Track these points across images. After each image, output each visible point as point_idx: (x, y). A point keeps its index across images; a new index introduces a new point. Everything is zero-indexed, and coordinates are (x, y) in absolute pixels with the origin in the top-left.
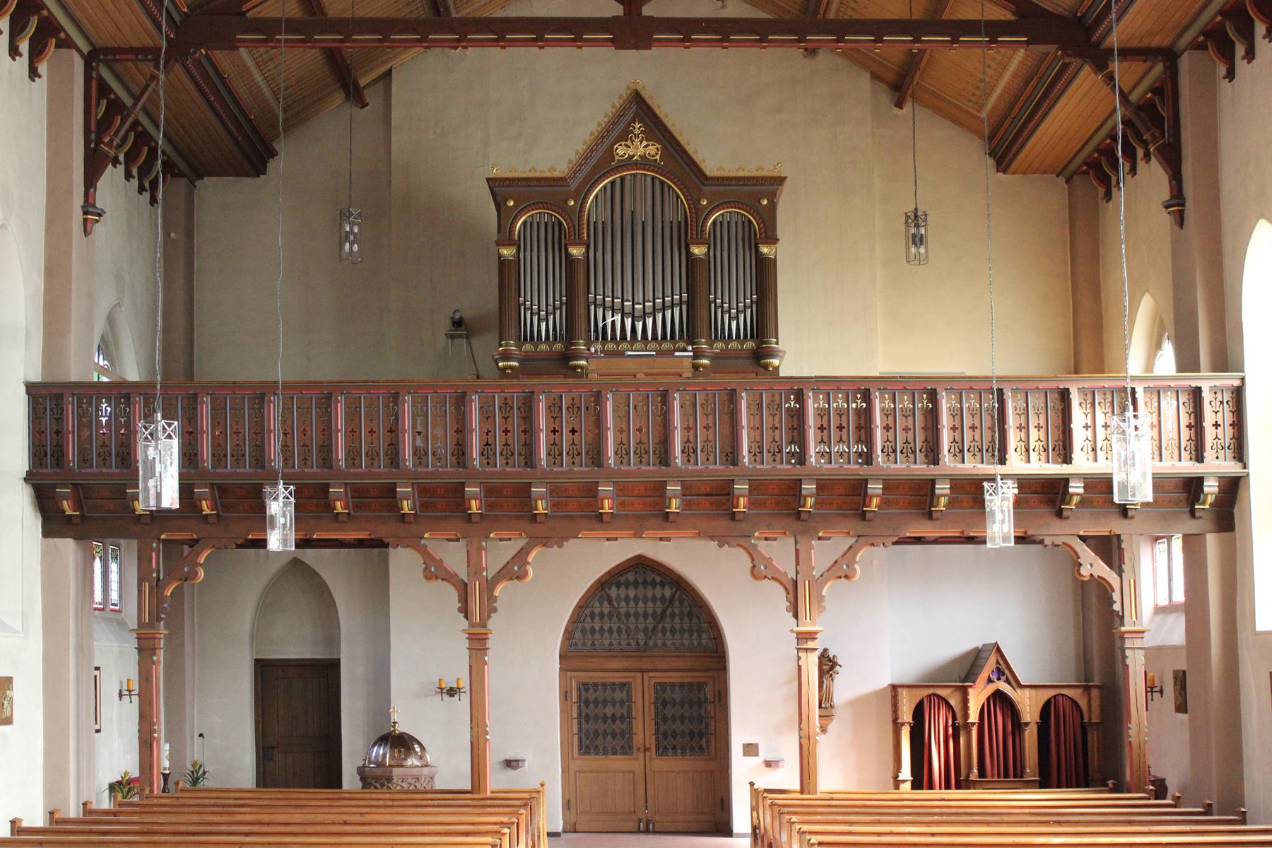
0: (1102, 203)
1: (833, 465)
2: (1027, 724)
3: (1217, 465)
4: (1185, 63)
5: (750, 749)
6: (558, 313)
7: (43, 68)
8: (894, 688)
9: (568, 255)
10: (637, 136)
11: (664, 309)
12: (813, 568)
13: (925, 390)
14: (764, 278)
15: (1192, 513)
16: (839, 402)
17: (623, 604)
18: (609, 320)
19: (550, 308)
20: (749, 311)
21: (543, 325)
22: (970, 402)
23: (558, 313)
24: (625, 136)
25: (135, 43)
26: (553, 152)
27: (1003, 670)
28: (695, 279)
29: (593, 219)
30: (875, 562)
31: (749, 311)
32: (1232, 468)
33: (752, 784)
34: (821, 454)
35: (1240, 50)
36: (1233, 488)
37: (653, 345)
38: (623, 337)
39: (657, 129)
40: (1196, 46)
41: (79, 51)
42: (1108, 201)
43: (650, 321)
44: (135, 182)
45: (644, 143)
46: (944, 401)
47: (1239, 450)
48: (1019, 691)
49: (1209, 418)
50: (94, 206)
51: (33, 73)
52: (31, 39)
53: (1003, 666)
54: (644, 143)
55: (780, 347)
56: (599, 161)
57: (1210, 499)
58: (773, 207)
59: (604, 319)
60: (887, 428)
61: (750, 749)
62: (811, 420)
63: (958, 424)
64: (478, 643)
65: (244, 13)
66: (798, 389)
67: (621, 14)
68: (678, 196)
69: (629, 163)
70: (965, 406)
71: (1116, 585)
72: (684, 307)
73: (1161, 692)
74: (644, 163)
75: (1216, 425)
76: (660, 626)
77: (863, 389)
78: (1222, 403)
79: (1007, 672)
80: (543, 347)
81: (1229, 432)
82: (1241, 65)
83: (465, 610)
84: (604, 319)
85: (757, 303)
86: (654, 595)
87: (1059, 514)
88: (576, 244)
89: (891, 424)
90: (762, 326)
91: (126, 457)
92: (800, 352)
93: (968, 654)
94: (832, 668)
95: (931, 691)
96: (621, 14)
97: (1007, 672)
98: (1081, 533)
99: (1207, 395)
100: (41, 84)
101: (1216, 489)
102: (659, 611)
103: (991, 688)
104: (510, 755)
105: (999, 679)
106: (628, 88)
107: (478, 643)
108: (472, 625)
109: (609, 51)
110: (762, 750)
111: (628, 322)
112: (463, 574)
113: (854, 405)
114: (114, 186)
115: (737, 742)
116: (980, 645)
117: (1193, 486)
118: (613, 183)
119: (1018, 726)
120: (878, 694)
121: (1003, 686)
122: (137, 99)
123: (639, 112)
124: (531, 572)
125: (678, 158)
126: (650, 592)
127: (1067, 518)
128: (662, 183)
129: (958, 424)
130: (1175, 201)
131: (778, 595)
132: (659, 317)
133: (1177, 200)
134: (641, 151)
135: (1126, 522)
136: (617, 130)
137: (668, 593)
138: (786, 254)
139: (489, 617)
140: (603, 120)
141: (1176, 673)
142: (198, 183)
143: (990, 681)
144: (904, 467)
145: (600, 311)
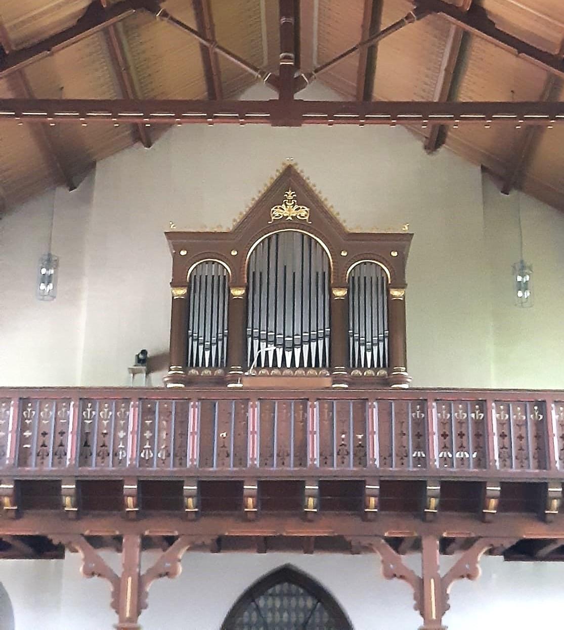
6: (220, 343)
10: (290, 201)
14: (395, 315)
16: (459, 413)
22: (517, 413)
23: (220, 343)
26: (222, 213)
28: (340, 318)
30: (494, 576)
34: (444, 460)
38: (275, 365)
39: (306, 196)
43: (297, 352)
46: (553, 412)
55: (281, 165)
56: (257, 218)
59: (259, 349)
60: (502, 436)
62: (435, 427)
67: (278, 99)
68: (323, 249)
69: (283, 222)
70: (513, 417)
72: (327, 340)
74: (296, 222)
77: (479, 400)
80: (207, 372)
83: (117, 605)
84: (259, 349)
85: (388, 337)
89: (507, 433)
90: (394, 357)
91: (5, 461)
92: (422, 371)
96: (278, 99)
106: (284, 164)
108: (122, 620)
109: (267, 127)
112: (119, 571)
113: (473, 415)
118: (269, 238)
123: (289, 181)
124: (180, 569)
128: (310, 238)
134: (294, 213)
138: (413, 296)
140: (263, 190)
144: (515, 471)
145: (256, 342)
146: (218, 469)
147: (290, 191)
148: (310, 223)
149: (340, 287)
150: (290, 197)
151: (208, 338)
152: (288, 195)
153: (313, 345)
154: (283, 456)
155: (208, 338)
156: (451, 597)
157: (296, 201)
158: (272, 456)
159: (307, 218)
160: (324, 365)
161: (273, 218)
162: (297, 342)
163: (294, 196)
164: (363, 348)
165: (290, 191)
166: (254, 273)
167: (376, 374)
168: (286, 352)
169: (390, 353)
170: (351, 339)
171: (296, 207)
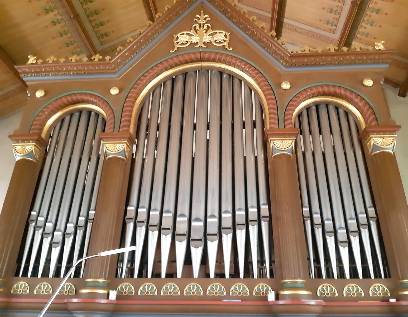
38: (171, 275)
147: (202, 15)
148: (231, 49)
149: (282, 135)
150: (202, 22)
151: (340, 222)
152: (199, 19)
153: (241, 235)
155: (340, 222)
156: (73, 227)
157: (209, 25)
159: (226, 44)
160: (261, 274)
161: (177, 46)
162: (197, 234)
163: (208, 19)
164: (331, 241)
165: (202, 15)
166: (149, 121)
167: (341, 292)
168: (193, 249)
169: (276, 242)
170: (308, 223)
171: (211, 32)
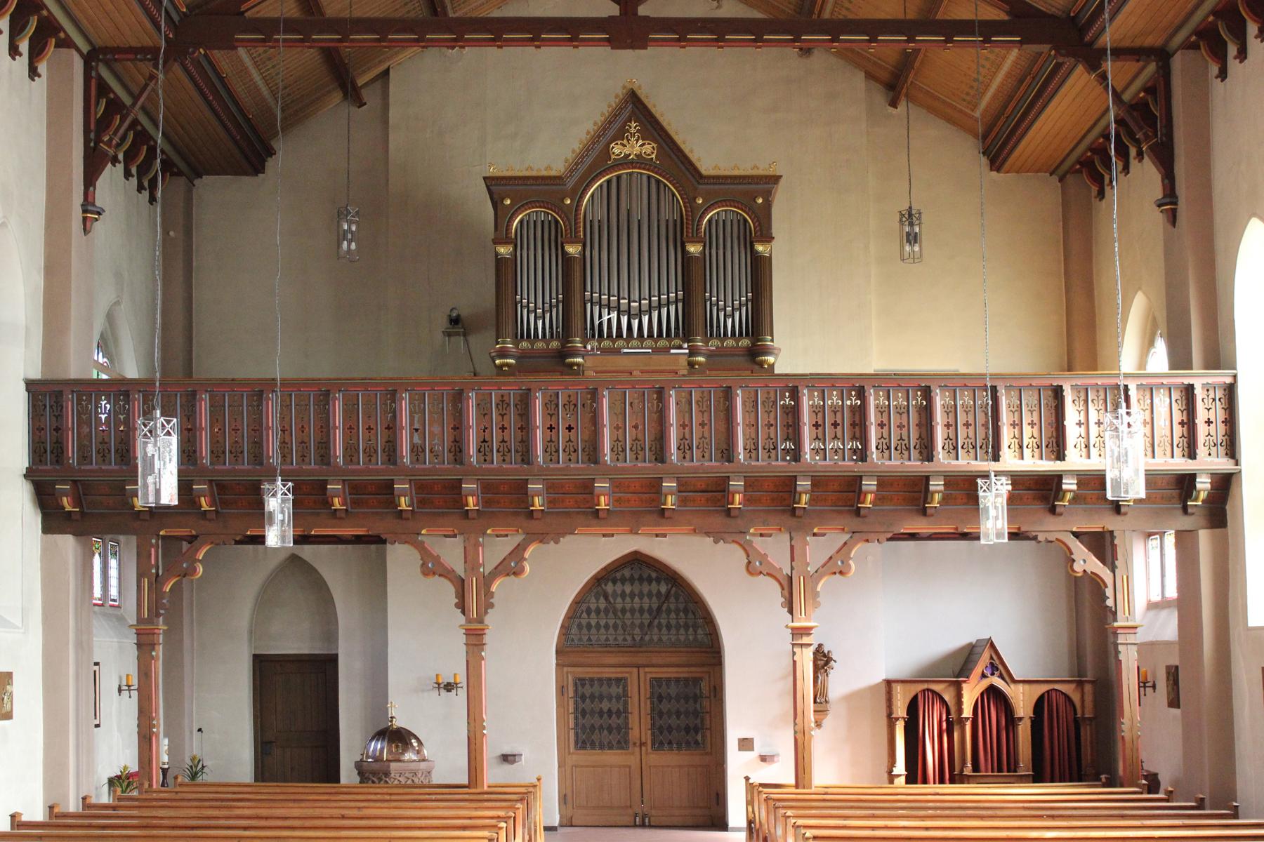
0: (1095, 202)
1: (828, 462)
2: (1020, 719)
3: (1209, 462)
4: (1177, 62)
5: (746, 744)
6: (554, 310)
7: (42, 68)
8: (889, 683)
9: (564, 253)
10: (633, 135)
11: (659, 307)
12: (808, 564)
13: (919, 388)
14: (759, 276)
15: (1185, 510)
16: (834, 399)
17: (619, 600)
18: (605, 318)
19: (547, 306)
20: (744, 309)
21: (540, 323)
22: (964, 399)
23: (554, 310)
24: (621, 135)
25: (134, 43)
26: (549, 151)
27: (997, 666)
28: (691, 277)
29: (589, 217)
30: (870, 558)
31: (744, 309)
32: (1224, 465)
33: (747, 779)
34: (816, 451)
35: (1232, 50)
36: (1225, 484)
37: (649, 343)
38: (619, 335)
39: (653, 128)
40: (1189, 46)
41: (78, 50)
42: (1101, 200)
43: (645, 319)
44: (134, 181)
45: (640, 142)
46: (938, 398)
47: (1231, 447)
48: (1012, 686)
49: (1201, 415)
50: (94, 205)
51: (33, 73)
52: (31, 39)
53: (997, 662)
54: (640, 142)
55: (776, 344)
56: (595, 160)
57: (1203, 496)
58: (768, 205)
59: (600, 317)
60: (881, 425)
61: (746, 744)
63: (952, 421)
64: (475, 638)
65: (243, 13)
66: (793, 386)
67: (617, 13)
68: (674, 195)
69: (625, 162)
71: (1109, 581)
72: (680, 305)
73: (1154, 687)
74: (640, 161)
75: (1209, 422)
76: (656, 622)
77: (858, 386)
78: (1214, 400)
79: (1000, 667)
80: (540, 345)
81: (1222, 429)
82: (1233, 65)
84: (600, 317)
85: (752, 301)
86: (650, 591)
87: (1053, 510)
88: (572, 242)
89: (885, 421)
90: (758, 324)
91: (125, 454)
92: (795, 349)
93: (962, 649)
94: (827, 663)
95: (925, 686)
96: (617, 13)
97: (1000, 667)
98: (1074, 529)
99: (1199, 392)
100: (41, 83)
101: (1209, 486)
102: (655, 606)
103: (985, 684)
104: (507, 750)
105: (993, 674)
106: (624, 87)
107: (475, 638)
108: (469, 621)
109: (605, 51)
110: (757, 745)
111: (624, 320)
112: (460, 570)
113: (849, 403)
114: (113, 185)
115: (732, 736)
116: (974, 641)
117: (1185, 483)
118: (609, 181)
119: (1011, 720)
120: (873, 689)
121: (997, 681)
122: (136, 99)
123: (635, 111)
124: (527, 568)
125: (673, 157)
126: (646, 588)
127: (1061, 514)
128: (658, 182)
129: (952, 421)
130: (1168, 200)
131: (773, 591)
132: (655, 314)
133: (1169, 199)
134: (637, 150)
135: (1119, 518)
136: (613, 129)
137: (663, 588)
138: (781, 252)
139: (486, 613)
140: (600, 119)
141: (1168, 668)
142: (197, 182)
143: (984, 676)
144: (898, 464)
145: (596, 309)
146: (373, 468)
154: (237, 454)
158: (224, 452)
